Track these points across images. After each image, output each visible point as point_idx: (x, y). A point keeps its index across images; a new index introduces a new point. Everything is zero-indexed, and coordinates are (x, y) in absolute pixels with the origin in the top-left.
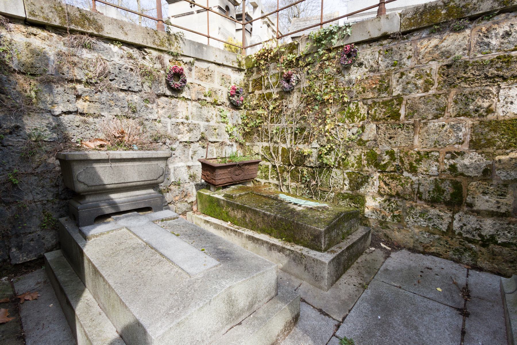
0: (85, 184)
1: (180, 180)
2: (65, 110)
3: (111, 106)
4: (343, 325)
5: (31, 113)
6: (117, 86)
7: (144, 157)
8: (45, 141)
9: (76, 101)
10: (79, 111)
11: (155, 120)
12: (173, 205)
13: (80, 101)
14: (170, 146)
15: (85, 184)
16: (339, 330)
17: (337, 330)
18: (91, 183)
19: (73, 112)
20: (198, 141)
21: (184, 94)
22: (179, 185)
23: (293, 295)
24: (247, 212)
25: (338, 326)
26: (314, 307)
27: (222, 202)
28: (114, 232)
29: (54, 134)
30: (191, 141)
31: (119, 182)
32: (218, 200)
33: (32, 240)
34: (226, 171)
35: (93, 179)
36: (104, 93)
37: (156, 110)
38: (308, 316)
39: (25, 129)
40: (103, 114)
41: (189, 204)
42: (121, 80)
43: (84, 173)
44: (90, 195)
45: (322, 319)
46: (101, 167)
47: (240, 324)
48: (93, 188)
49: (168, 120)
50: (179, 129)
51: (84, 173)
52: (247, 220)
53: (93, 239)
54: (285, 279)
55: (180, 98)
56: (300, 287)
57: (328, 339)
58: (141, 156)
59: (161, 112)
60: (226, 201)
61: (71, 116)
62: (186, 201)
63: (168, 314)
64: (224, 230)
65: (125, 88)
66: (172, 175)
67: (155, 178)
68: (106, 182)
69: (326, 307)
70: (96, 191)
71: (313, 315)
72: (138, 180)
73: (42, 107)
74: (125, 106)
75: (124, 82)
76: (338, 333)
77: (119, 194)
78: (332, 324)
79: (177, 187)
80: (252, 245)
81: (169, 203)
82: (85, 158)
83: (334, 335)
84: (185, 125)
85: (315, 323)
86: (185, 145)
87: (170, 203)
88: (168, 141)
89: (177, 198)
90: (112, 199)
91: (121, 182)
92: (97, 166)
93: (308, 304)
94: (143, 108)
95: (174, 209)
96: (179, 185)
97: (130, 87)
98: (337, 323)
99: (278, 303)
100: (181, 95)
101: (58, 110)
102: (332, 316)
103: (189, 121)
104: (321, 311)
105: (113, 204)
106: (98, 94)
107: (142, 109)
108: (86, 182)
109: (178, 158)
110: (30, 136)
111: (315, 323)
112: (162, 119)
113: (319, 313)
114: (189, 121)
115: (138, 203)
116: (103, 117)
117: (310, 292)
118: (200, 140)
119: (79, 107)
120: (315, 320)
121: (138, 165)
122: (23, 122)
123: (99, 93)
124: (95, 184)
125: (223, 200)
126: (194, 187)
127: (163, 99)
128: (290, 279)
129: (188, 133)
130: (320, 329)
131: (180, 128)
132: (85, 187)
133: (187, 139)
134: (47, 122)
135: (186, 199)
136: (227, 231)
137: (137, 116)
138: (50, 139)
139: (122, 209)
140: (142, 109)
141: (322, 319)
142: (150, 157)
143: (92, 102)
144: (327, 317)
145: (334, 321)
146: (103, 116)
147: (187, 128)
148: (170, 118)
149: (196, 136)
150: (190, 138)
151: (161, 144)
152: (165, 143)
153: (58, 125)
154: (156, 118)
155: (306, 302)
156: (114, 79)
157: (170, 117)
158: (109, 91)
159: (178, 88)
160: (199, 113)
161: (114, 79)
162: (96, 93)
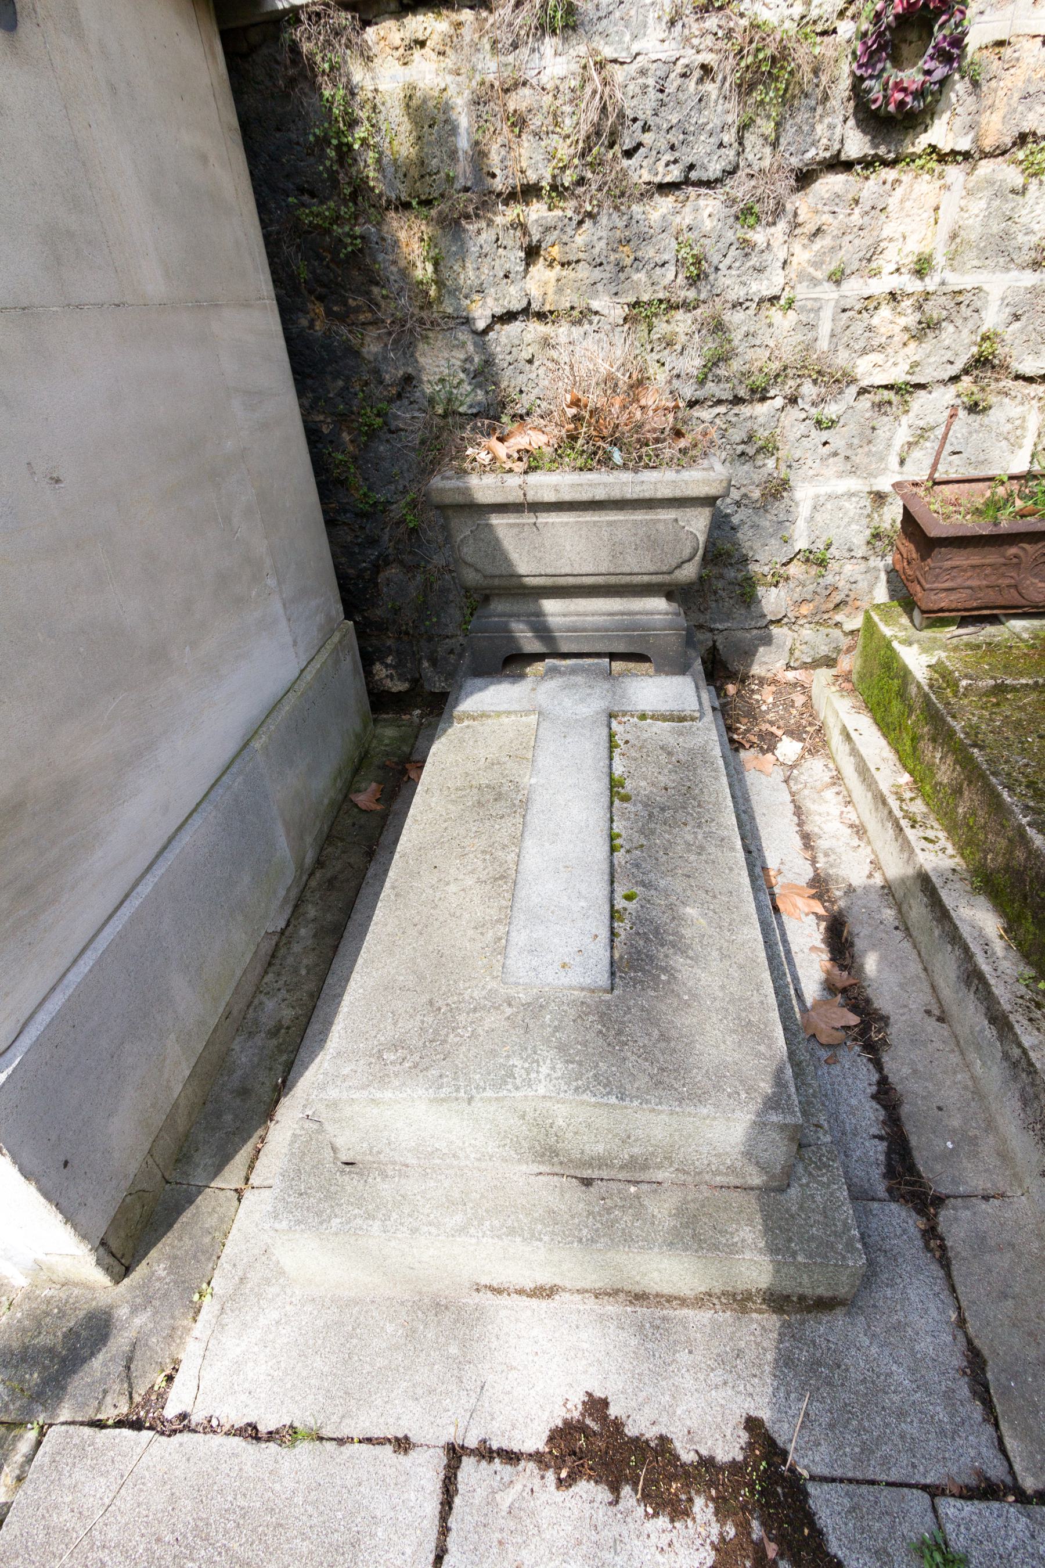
0: (477, 570)
1: (829, 546)
2: (499, 311)
3: (622, 269)
4: (1010, 1509)
5: (431, 334)
6: (646, 177)
7: (629, 496)
8: (460, 414)
9: (526, 271)
10: (535, 307)
11: (774, 299)
12: (785, 629)
13: (538, 269)
14: (813, 411)
15: (477, 570)
16: (969, 1508)
17: (968, 1494)
18: (490, 570)
19: (518, 313)
20: (955, 379)
21: (940, 133)
22: (822, 563)
23: (832, 1246)
24: (970, 782)
25: (985, 1491)
26: (962, 1322)
27: (913, 690)
28: (513, 717)
29: (479, 392)
30: (915, 380)
31: (558, 572)
32: (905, 674)
33: (452, 652)
34: (976, 560)
35: (494, 558)
36: (603, 220)
37: (782, 255)
38: (898, 1327)
39: (421, 381)
40: (595, 305)
41: (846, 634)
42: (662, 144)
43: (471, 541)
44: (499, 595)
45: (948, 1395)
46: (512, 526)
47: (587, 1182)
48: (497, 582)
49: (829, 293)
50: (870, 329)
51: (471, 541)
52: (960, 810)
53: (466, 723)
54: (956, 1123)
55: (913, 158)
56: (984, 1206)
57: (894, 1476)
58: (616, 494)
59: (803, 255)
60: (926, 696)
61: (514, 328)
62: (837, 624)
63: (380, 1057)
64: (875, 797)
65: (675, 174)
66: (801, 525)
67: (665, 569)
68: (522, 569)
69: (1015, 1376)
70: (505, 588)
71: (925, 1345)
72: (612, 570)
73: (450, 310)
74: (666, 257)
75: (672, 148)
76: (950, 1508)
77: (567, 601)
78: (971, 1453)
79: (814, 570)
80: (924, 911)
81: (772, 622)
82: (460, 499)
83: (934, 1491)
84: (907, 303)
85: (900, 1374)
86: (879, 406)
87: (779, 621)
88: (808, 390)
89: (805, 609)
90: (511, 632)
91: (563, 571)
92: (497, 521)
93: (953, 1289)
94: (733, 253)
95: (789, 644)
96: (822, 563)
97: (691, 167)
98: (996, 1471)
99: (750, 1222)
100: (924, 140)
101: (481, 314)
102: (1004, 1426)
103: (931, 283)
104: (975, 1363)
105: (543, 631)
106: (585, 226)
107: (727, 261)
108: (480, 566)
109: (840, 459)
110: (432, 401)
111: (900, 1374)
112: (802, 292)
113: (958, 1361)
114: (931, 283)
115: (609, 638)
116: (596, 319)
117: (1003, 1261)
118: (966, 372)
119: (535, 292)
120: (912, 1371)
121: (610, 524)
122: (417, 361)
123: (588, 224)
124: (498, 573)
125: (919, 686)
126: (883, 577)
127: (831, 183)
128: (973, 1141)
129: (913, 345)
130: (901, 1415)
131: (875, 321)
132: (478, 577)
133: (897, 374)
134: (462, 356)
135: (839, 617)
136: (881, 806)
137: (702, 296)
138: (471, 406)
139: (565, 648)
140: (727, 261)
141: (948, 1395)
142: (647, 495)
143: (569, 263)
144: (977, 1410)
145: (990, 1453)
146: (596, 313)
147: (911, 319)
148: (838, 283)
149: (949, 355)
150: (915, 365)
151: (779, 402)
152: (793, 400)
153: (486, 362)
154: (775, 291)
155: (949, 1276)
156: (640, 145)
157: (837, 278)
158: (616, 208)
159: (902, 104)
160: (996, 228)
161: (640, 145)
162: (581, 223)
